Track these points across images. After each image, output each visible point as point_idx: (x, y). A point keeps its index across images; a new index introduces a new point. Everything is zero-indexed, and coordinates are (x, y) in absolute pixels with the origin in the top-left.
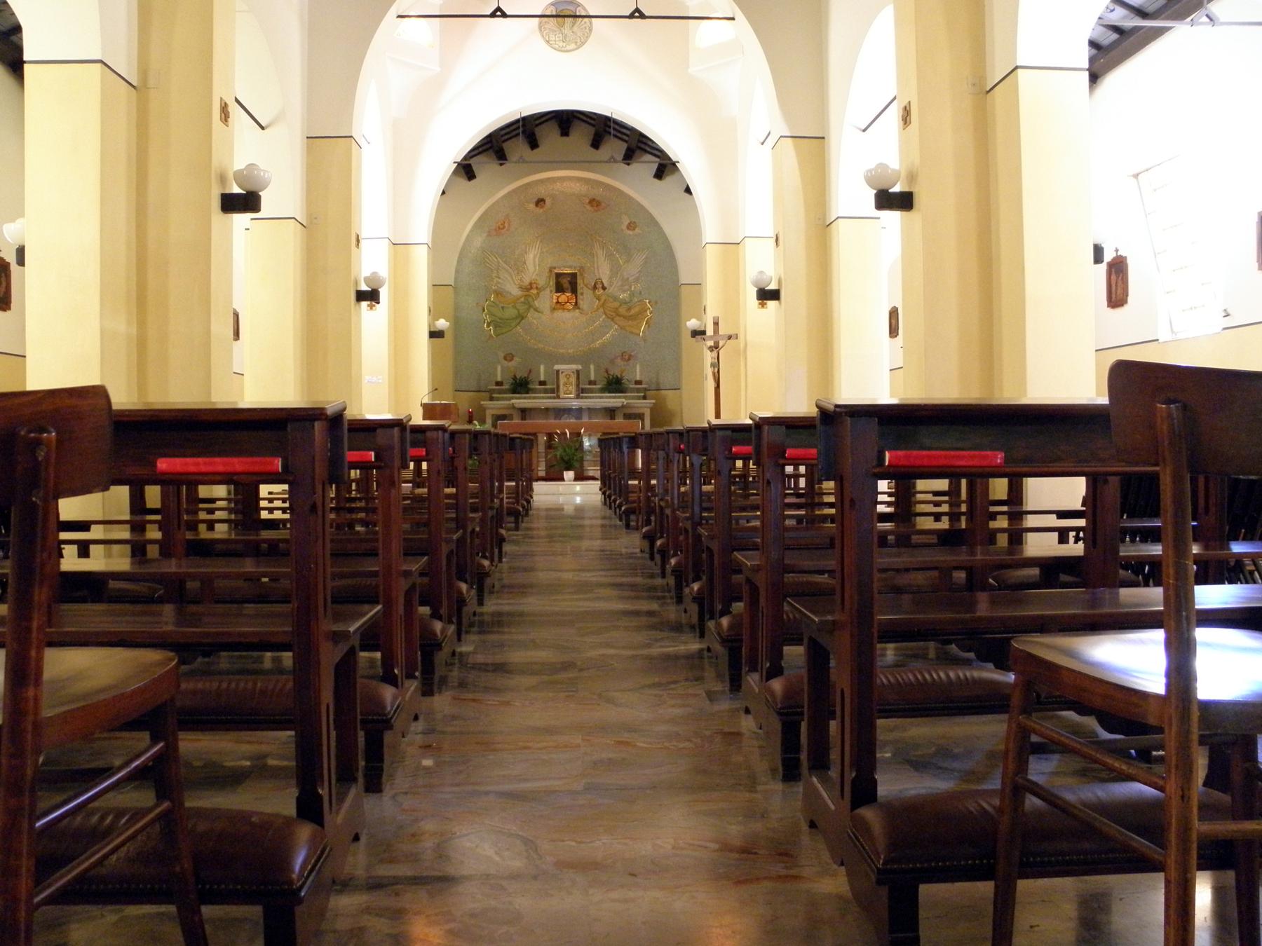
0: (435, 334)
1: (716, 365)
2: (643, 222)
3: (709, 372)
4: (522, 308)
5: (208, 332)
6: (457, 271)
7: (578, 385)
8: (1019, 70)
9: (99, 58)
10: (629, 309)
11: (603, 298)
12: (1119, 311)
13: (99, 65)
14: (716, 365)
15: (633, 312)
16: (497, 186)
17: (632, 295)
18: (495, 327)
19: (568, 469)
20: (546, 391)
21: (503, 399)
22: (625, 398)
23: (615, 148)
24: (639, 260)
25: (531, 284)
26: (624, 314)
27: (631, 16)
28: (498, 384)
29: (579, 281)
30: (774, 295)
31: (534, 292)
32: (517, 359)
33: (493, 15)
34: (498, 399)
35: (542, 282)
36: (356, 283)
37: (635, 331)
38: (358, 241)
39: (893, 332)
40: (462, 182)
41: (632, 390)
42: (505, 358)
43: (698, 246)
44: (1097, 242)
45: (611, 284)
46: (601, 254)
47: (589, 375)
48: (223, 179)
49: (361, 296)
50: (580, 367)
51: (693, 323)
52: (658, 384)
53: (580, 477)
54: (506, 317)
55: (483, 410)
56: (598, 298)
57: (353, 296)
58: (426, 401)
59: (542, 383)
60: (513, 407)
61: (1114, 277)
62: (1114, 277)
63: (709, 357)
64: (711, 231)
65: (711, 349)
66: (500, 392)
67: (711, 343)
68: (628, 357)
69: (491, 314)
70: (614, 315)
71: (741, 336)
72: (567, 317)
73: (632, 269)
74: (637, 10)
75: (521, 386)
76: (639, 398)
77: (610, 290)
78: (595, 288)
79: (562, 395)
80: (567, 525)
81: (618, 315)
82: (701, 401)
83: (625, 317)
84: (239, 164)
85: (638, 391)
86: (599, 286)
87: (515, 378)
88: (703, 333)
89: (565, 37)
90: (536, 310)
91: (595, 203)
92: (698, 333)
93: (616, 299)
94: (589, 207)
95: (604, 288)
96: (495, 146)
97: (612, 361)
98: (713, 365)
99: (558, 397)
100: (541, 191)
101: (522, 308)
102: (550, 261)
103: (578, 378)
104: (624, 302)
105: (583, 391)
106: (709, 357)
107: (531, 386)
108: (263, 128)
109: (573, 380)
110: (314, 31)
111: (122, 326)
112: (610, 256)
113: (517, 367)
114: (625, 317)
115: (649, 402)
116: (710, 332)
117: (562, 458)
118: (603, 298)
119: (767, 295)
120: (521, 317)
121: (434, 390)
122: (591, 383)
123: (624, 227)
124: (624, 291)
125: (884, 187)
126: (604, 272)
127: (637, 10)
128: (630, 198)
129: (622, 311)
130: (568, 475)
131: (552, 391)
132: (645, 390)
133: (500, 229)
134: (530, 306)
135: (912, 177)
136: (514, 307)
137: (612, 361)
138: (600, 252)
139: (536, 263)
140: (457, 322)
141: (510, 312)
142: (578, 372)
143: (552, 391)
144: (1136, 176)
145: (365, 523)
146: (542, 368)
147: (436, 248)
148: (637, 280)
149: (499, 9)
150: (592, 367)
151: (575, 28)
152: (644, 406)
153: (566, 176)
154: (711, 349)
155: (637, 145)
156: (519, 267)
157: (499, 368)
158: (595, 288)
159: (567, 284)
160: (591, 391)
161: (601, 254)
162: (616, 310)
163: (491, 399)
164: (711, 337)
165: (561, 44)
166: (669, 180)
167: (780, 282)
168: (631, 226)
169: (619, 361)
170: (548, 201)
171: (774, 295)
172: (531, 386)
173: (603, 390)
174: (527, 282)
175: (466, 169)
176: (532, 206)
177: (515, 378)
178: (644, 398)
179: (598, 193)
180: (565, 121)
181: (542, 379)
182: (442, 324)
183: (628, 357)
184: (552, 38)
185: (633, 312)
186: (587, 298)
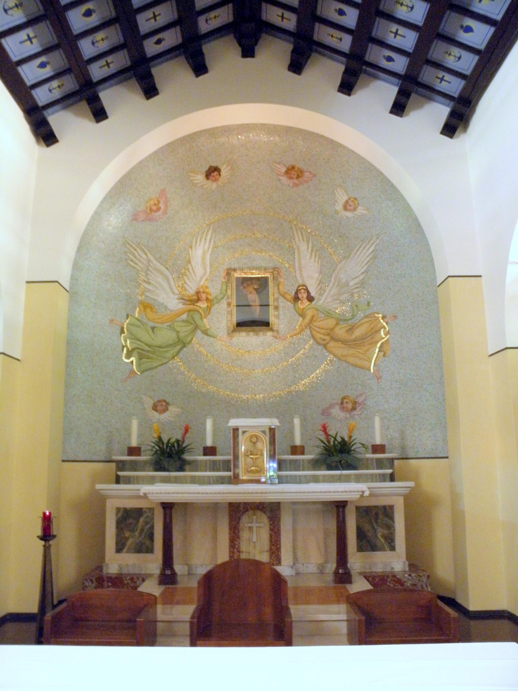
4: (184, 330)
10: (351, 329)
11: (309, 314)
15: (357, 333)
17: (356, 306)
18: (140, 358)
20: (214, 466)
22: (358, 479)
25: (198, 293)
26: (347, 337)
28: (133, 451)
31: (203, 305)
35: (214, 290)
37: (365, 363)
42: (155, 408)
45: (321, 291)
50: (275, 422)
52: (403, 448)
54: (158, 346)
56: (302, 315)
59: (210, 451)
69: (134, 338)
70: (327, 340)
72: (248, 339)
73: (353, 269)
75: (170, 456)
77: (320, 302)
78: (296, 298)
79: (243, 477)
81: (333, 339)
83: (344, 342)
85: (380, 463)
86: (303, 295)
90: (205, 332)
93: (329, 314)
94: (284, 179)
95: (310, 299)
97: (326, 412)
99: (235, 480)
101: (184, 330)
102: (228, 260)
107: (187, 457)
109: (264, 447)
113: (168, 425)
114: (344, 342)
118: (309, 314)
120: (182, 343)
122: (295, 450)
123: (339, 207)
124: (343, 303)
126: (308, 271)
129: (340, 332)
131: (226, 466)
132: (391, 461)
133: (152, 211)
134: (197, 327)
136: (171, 328)
137: (326, 412)
138: (303, 246)
139: (207, 261)
141: (164, 336)
142: (272, 431)
143: (226, 466)
145: (320, 377)
150: (297, 422)
156: (181, 269)
158: (296, 298)
163: (118, 480)
169: (336, 411)
170: (225, 171)
172: (187, 457)
173: (315, 464)
174: (191, 289)
176: (200, 178)
178: (392, 478)
181: (209, 443)
183: (351, 405)
185: (357, 333)
186: (282, 316)
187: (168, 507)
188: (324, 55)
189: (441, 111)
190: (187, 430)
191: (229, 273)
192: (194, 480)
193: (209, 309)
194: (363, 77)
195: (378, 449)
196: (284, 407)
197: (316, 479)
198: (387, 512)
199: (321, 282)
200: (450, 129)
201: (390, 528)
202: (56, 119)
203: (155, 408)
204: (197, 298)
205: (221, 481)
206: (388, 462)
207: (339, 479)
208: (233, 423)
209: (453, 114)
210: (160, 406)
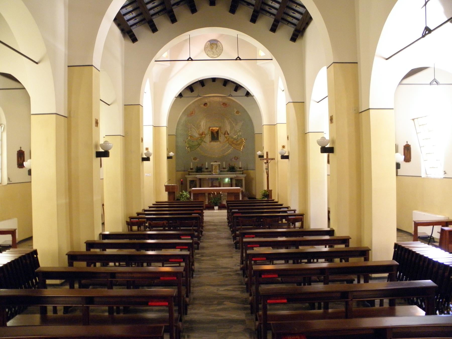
0: (169, 158)
1: (267, 169)
2: (241, 111)
3: (265, 171)
5: (93, 199)
6: (177, 129)
7: (219, 170)
8: (370, 110)
9: (55, 112)
10: (237, 141)
11: (228, 138)
12: (408, 163)
13: (55, 115)
14: (267, 169)
15: (238, 142)
16: (190, 101)
17: (238, 136)
18: (190, 148)
19: (216, 206)
20: (208, 172)
21: (194, 175)
22: (236, 174)
23: (230, 88)
24: (240, 124)
25: (202, 133)
26: (235, 143)
27: (236, 59)
28: (191, 169)
29: (219, 132)
30: (287, 157)
31: (204, 135)
32: (198, 160)
33: (188, 60)
34: (191, 175)
35: (206, 132)
36: (142, 155)
38: (142, 140)
39: (328, 162)
40: (179, 99)
41: (238, 171)
42: (194, 159)
43: (262, 126)
44: (398, 162)
46: (227, 122)
47: (223, 165)
48: (96, 146)
49: (144, 159)
50: (219, 163)
51: (259, 153)
52: (247, 168)
53: (221, 207)
54: (194, 145)
55: (186, 179)
56: (226, 138)
57: (141, 160)
58: (166, 184)
59: (207, 169)
60: (196, 178)
61: (406, 151)
62: (406, 151)
63: (265, 166)
64: (265, 121)
65: (265, 163)
66: (192, 172)
67: (265, 161)
68: (237, 158)
69: (188, 143)
70: (232, 144)
71: (276, 159)
72: (214, 144)
73: (238, 128)
74: (238, 57)
75: (199, 170)
76: (240, 174)
78: (225, 134)
80: (216, 226)
81: (233, 143)
82: (262, 183)
83: (236, 145)
84: (102, 142)
85: (240, 171)
87: (197, 167)
88: (263, 156)
89: (214, 52)
90: (204, 142)
91: (225, 104)
92: (261, 156)
93: (232, 138)
94: (222, 106)
95: (228, 134)
96: (190, 88)
97: (231, 160)
98: (266, 169)
100: (206, 101)
103: (219, 167)
104: (235, 139)
105: (221, 171)
106: (265, 166)
107: (203, 170)
108: (109, 105)
109: (218, 168)
110: (126, 69)
111: (64, 201)
112: (230, 123)
115: (244, 175)
116: (265, 157)
117: (214, 202)
118: (228, 138)
119: (284, 157)
120: (199, 145)
121: (169, 180)
122: (224, 168)
123: (235, 113)
124: (235, 135)
125: (324, 146)
126: (228, 128)
127: (238, 57)
128: (237, 103)
129: (235, 142)
130: (216, 208)
131: (210, 172)
134: (202, 141)
135: (333, 142)
137: (231, 160)
138: (227, 121)
139: (204, 125)
140: (177, 154)
141: (196, 143)
142: (219, 165)
143: (210, 172)
144: (413, 120)
146: (207, 163)
147: (168, 128)
148: (240, 131)
149: (190, 58)
150: (224, 163)
151: (217, 49)
152: (242, 177)
153: (215, 97)
154: (265, 163)
155: (238, 87)
156: (198, 127)
157: (192, 163)
158: (225, 134)
159: (215, 136)
160: (224, 171)
161: (227, 122)
162: (232, 142)
163: (189, 175)
164: (265, 159)
165: (212, 55)
166: (249, 97)
167: (289, 153)
168: (237, 112)
169: (233, 160)
170: (208, 104)
171: (287, 157)
172: (203, 170)
173: (228, 171)
175: (180, 95)
176: (203, 106)
177: (197, 167)
178: (243, 174)
179: (225, 101)
180: (214, 80)
181: (207, 167)
182: (171, 154)
183: (237, 158)
184: (209, 53)
185: (238, 142)
186: (222, 138)
187: (200, 179)
188: (243, 5)
189: (290, 30)
190: (202, 165)
191: (209, 128)
192: (204, 174)
193: (205, 136)
194: (260, 15)
195: (240, 168)
196: (222, 159)
197: (228, 174)
198: (241, 180)
199: (230, 130)
200: (294, 39)
201: (242, 183)
202: (135, 30)
203: (194, 159)
204: (202, 134)
205: (209, 174)
206: (243, 170)
207: (232, 174)
208: (212, 163)
209: (296, 30)
210: (195, 159)
